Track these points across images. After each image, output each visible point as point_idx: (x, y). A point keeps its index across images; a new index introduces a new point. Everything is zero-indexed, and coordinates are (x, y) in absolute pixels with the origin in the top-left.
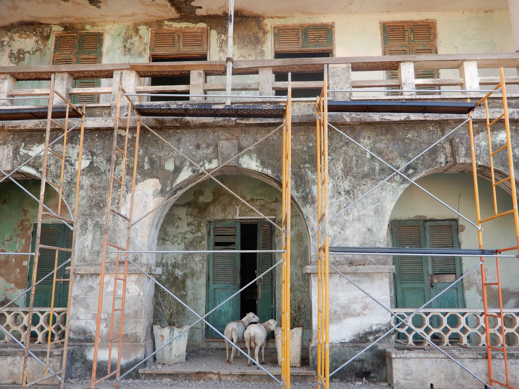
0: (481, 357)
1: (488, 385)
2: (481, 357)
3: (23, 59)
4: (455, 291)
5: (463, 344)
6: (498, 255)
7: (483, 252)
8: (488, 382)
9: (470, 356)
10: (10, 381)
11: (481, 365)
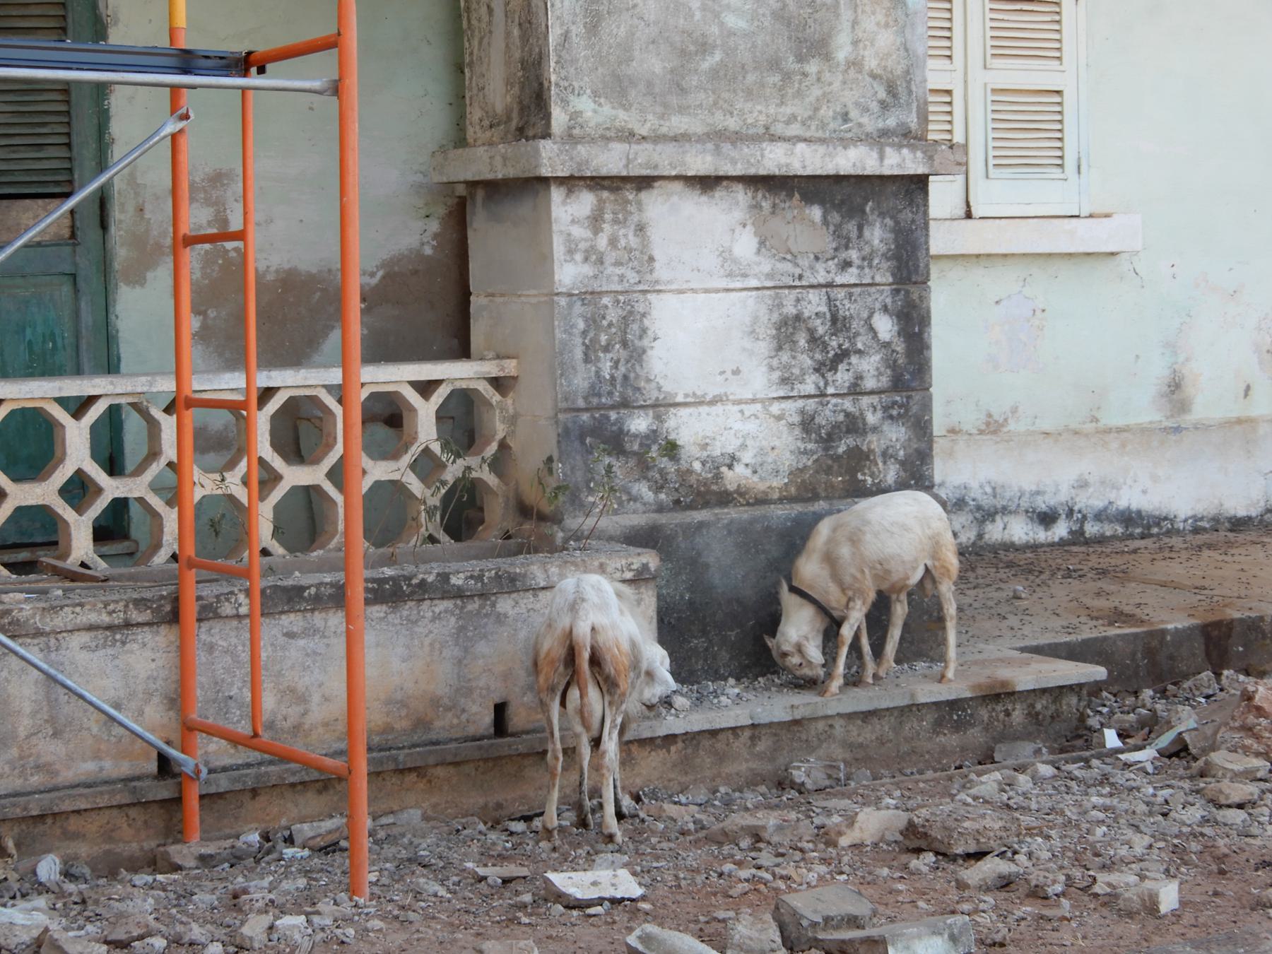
0: (146, 616)
1: (173, 753)
2: (146, 616)
4: (66, 289)
5: (72, 562)
6: (254, 80)
7: (187, 61)
8: (175, 736)
9: (93, 618)
11: (148, 655)
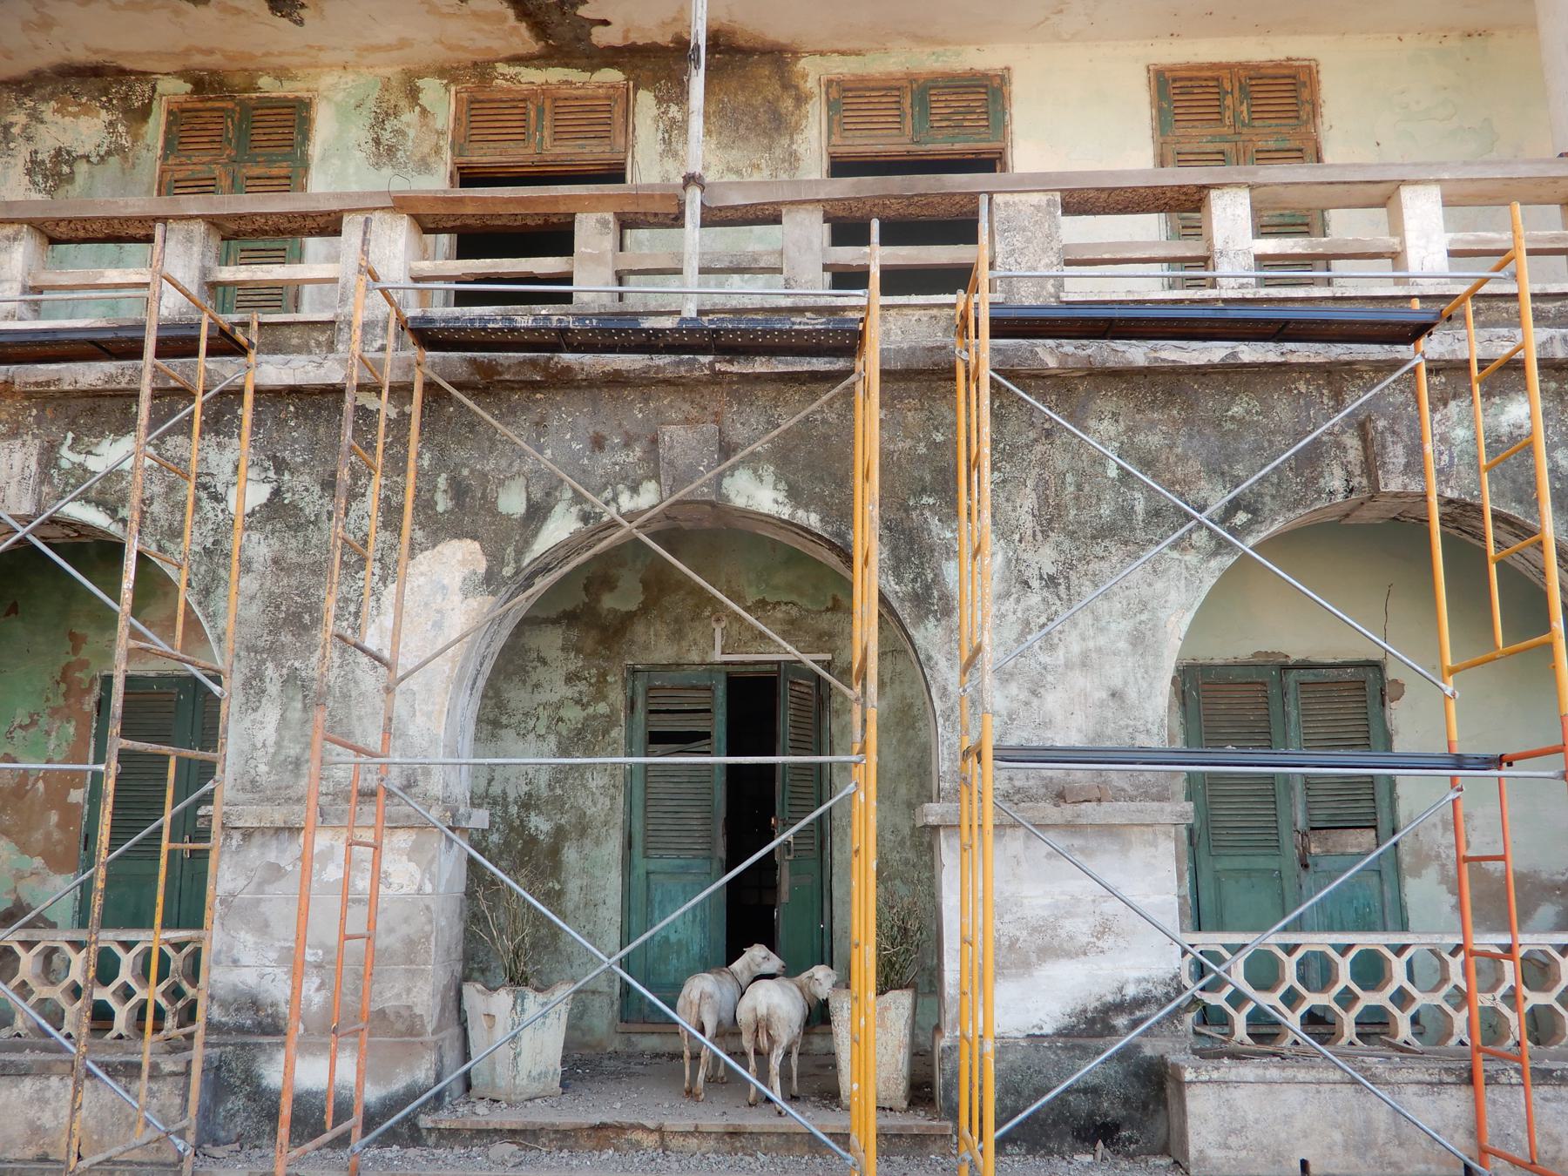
0: (1452, 1079)
1: (1475, 1165)
2: (1452, 1079)
3: (70, 178)
4: (1375, 879)
5: (1399, 1040)
6: (1505, 771)
7: (1459, 762)
8: (1475, 1154)
9: (1420, 1077)
10: (31, 1152)
11: (1454, 1103)
